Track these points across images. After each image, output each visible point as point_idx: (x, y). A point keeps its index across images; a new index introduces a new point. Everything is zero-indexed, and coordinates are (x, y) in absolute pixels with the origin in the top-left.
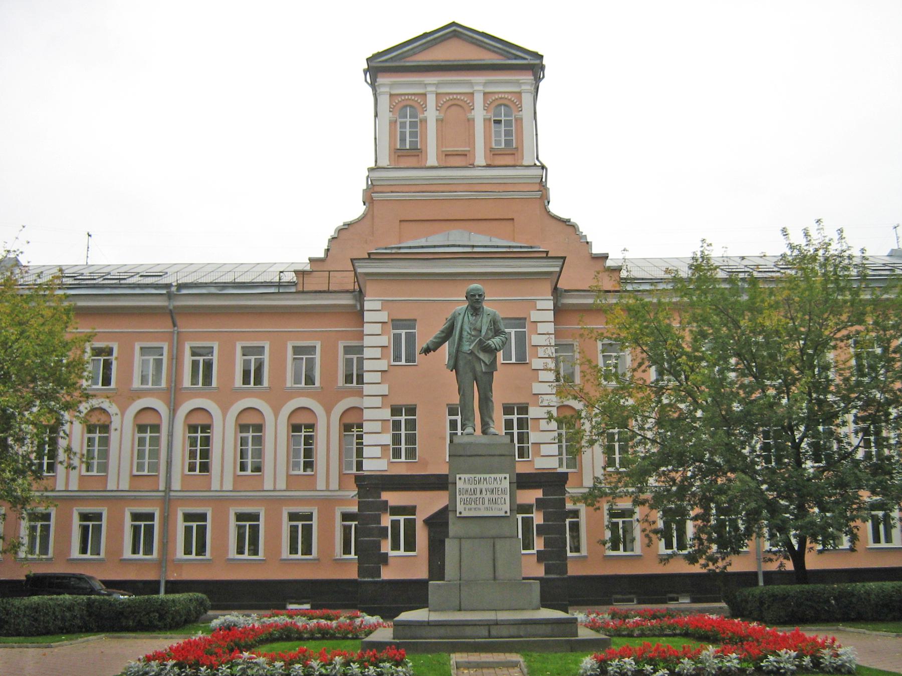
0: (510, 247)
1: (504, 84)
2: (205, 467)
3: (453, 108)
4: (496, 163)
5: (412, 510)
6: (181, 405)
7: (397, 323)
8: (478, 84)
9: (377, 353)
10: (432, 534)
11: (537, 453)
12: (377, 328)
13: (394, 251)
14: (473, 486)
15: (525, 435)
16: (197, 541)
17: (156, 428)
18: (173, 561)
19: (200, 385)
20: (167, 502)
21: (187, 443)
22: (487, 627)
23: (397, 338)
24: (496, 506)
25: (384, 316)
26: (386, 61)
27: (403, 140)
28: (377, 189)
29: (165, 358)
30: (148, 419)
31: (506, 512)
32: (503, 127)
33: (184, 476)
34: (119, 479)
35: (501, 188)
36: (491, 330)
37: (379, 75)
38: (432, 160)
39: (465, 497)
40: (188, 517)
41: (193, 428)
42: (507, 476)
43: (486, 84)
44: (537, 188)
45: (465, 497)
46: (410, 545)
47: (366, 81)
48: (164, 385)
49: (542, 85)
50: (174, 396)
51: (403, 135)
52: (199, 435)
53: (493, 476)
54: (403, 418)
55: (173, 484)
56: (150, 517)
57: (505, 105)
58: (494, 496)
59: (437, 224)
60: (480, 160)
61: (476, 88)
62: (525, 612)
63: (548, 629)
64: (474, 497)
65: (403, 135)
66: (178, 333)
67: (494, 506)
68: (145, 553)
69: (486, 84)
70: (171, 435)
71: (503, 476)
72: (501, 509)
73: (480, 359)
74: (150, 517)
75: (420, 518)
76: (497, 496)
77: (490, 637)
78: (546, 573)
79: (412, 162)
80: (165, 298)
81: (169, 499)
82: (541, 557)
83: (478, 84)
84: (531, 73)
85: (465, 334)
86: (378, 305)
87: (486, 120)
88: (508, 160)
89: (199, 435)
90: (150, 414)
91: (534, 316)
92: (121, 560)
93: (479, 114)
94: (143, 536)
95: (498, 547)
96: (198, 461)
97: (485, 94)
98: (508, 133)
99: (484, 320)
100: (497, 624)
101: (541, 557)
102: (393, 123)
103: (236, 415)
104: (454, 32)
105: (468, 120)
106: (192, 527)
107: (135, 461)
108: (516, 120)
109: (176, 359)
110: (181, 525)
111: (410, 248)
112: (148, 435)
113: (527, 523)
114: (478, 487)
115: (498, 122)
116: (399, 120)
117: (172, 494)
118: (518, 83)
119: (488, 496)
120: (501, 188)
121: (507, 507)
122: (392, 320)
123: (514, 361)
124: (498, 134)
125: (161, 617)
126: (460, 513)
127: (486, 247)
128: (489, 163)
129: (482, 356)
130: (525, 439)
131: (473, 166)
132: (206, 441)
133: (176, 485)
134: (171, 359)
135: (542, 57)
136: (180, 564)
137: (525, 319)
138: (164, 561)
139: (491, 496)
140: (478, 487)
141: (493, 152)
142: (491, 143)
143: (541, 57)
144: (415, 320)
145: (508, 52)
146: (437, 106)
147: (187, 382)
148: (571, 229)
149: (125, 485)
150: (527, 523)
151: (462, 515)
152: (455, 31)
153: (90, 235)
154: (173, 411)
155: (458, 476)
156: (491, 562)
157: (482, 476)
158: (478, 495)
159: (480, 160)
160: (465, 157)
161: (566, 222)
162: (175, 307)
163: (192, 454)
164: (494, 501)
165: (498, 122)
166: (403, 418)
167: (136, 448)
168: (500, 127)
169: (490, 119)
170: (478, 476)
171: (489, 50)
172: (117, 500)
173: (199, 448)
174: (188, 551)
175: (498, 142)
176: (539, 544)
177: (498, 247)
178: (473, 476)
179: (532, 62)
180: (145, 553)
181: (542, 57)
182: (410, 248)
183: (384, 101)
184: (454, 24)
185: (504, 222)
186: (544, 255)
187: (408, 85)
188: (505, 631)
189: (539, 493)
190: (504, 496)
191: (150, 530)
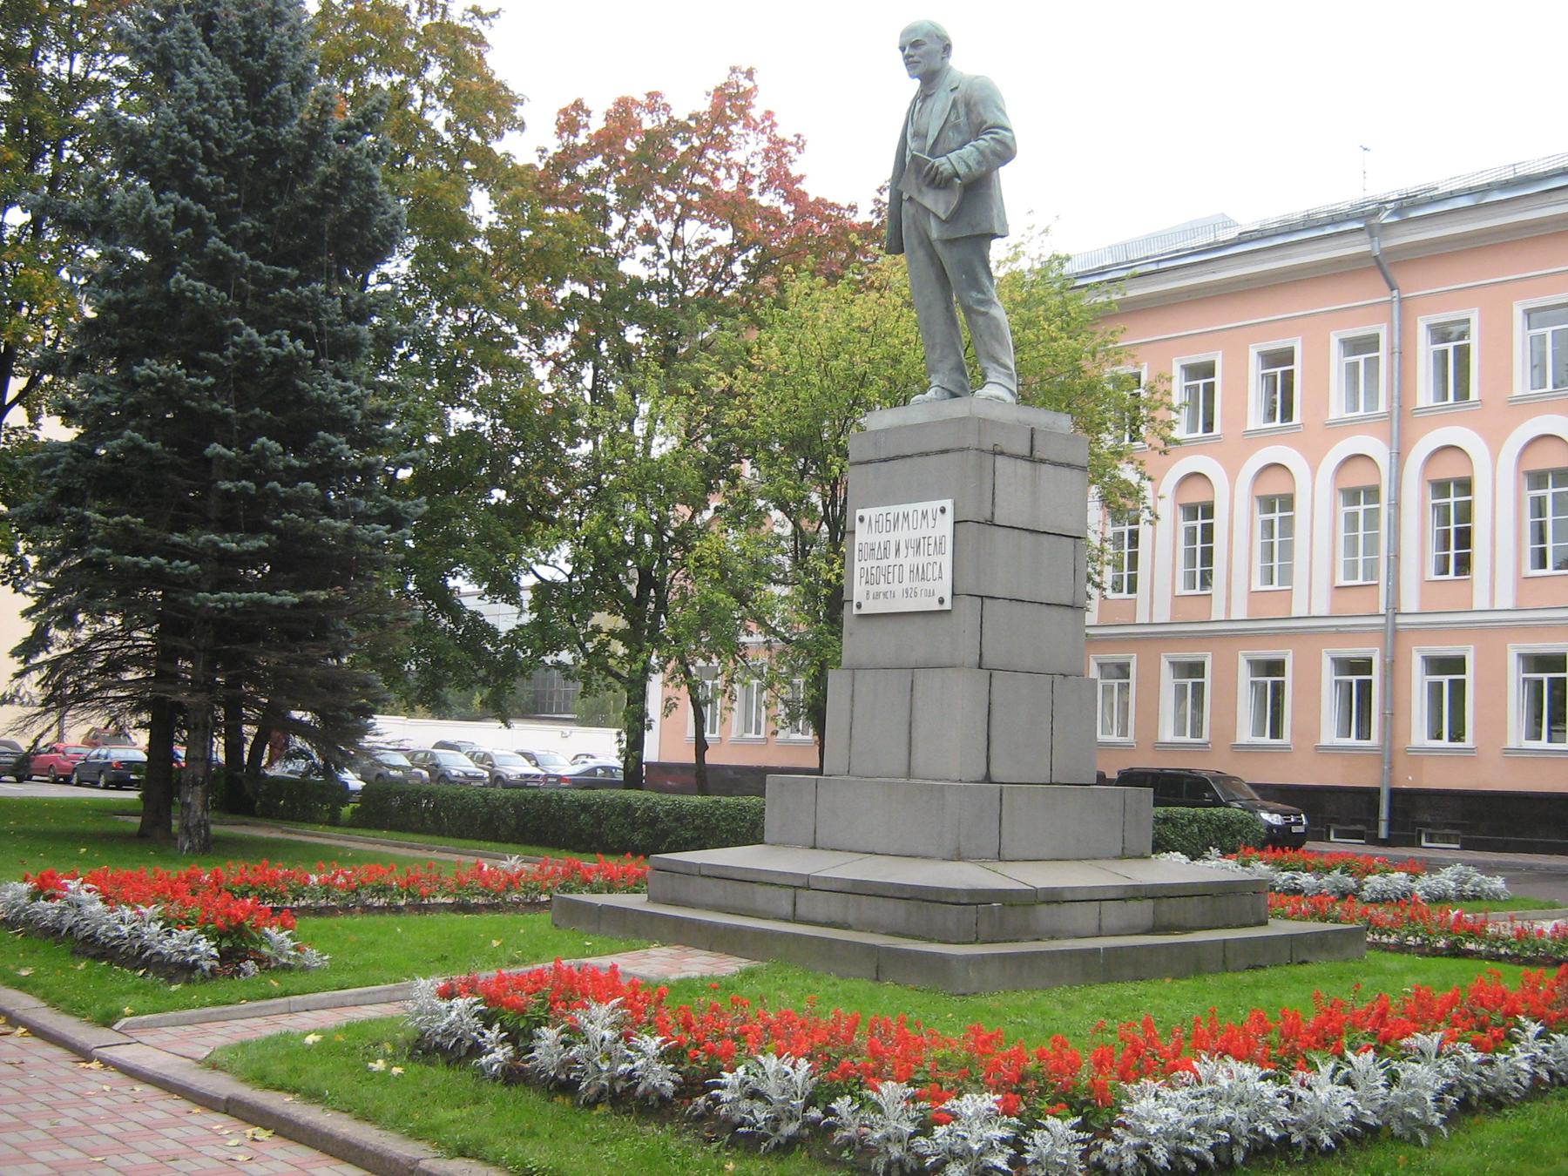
2: (1464, 564)
14: (884, 537)
15: (1536, 384)
16: (1450, 714)
17: (1372, 493)
19: (1550, 387)
20: (1394, 635)
21: (1431, 517)
22: (791, 891)
30: (1358, 477)
31: (941, 601)
34: (1311, 597)
36: (956, 127)
41: (1440, 488)
42: (948, 504)
48: (1382, 407)
50: (1401, 425)
52: (1452, 500)
58: (922, 560)
63: (894, 912)
64: (884, 563)
67: (921, 585)
68: (1359, 737)
70: (1396, 505)
71: (938, 504)
72: (931, 594)
77: (794, 919)
80: (1364, 237)
81: (1395, 631)
90: (1360, 465)
92: (1317, 748)
95: (918, 689)
96: (1452, 552)
100: (808, 888)
103: (1518, 450)
106: (1440, 684)
109: (1403, 354)
112: (1361, 508)
114: (893, 537)
119: (908, 560)
126: (859, 606)
136: (1422, 754)
138: (1389, 754)
140: (893, 537)
147: (1424, 394)
149: (1321, 606)
151: (863, 611)
154: (1399, 457)
162: (1387, 252)
164: (919, 573)
167: (1341, 534)
172: (1306, 633)
173: (1452, 527)
178: (883, 510)
180: (1359, 737)
191: (1365, 688)
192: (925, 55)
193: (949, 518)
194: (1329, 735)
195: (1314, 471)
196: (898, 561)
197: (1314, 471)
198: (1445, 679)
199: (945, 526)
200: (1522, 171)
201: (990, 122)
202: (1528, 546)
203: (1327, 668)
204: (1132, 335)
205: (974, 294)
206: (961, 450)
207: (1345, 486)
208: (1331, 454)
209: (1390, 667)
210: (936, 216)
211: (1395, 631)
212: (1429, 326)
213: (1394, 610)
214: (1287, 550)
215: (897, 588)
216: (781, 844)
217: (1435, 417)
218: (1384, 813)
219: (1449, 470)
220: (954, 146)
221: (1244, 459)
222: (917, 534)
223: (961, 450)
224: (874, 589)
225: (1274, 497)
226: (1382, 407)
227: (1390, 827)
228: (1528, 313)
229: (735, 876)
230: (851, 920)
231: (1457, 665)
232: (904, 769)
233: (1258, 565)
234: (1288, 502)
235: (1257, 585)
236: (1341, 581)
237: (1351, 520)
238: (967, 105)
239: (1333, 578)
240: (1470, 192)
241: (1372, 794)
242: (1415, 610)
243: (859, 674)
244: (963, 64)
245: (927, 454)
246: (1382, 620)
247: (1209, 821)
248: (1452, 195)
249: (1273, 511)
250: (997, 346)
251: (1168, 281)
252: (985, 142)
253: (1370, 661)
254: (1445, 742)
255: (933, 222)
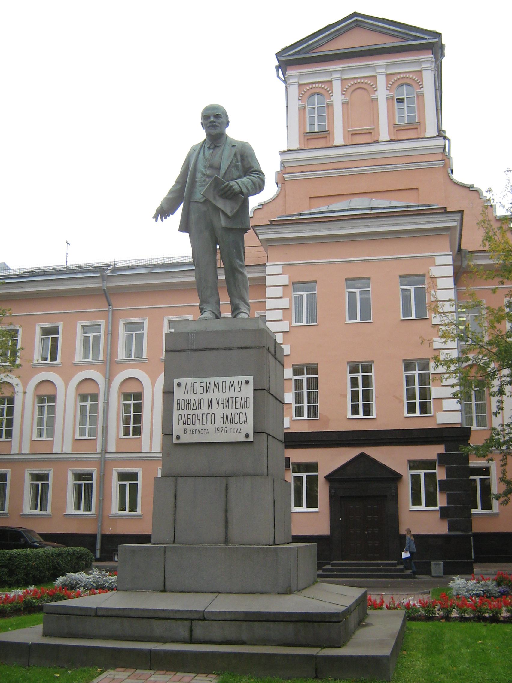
0: (408, 207)
1: (403, 65)
2: (137, 431)
3: (358, 91)
4: (400, 138)
5: (312, 467)
6: (116, 375)
7: (297, 285)
8: (380, 66)
9: (279, 315)
10: (333, 491)
11: (440, 408)
12: (279, 292)
13: (294, 218)
14: (198, 397)
16: (40, 496)
17: (95, 397)
18: (109, 516)
23: (299, 299)
24: (233, 426)
25: (285, 280)
26: (293, 54)
27: (312, 125)
28: (288, 170)
29: (102, 334)
30: (88, 389)
31: (247, 436)
32: (405, 104)
33: (119, 439)
34: (63, 442)
35: (405, 160)
36: (236, 167)
37: (288, 68)
38: (339, 139)
39: (186, 412)
40: (123, 477)
41: (126, 396)
42: (251, 378)
43: (387, 66)
44: (440, 157)
45: (186, 412)
46: (313, 502)
47: (278, 76)
48: (101, 358)
49: (445, 62)
50: (110, 367)
51: (312, 119)
53: (228, 379)
54: (305, 377)
55: (108, 448)
56: (90, 476)
57: (407, 84)
59: (345, 197)
60: (384, 135)
61: (378, 71)
62: (264, 598)
65: (312, 119)
66: (113, 311)
69: (387, 66)
70: (107, 403)
71: (244, 378)
72: (239, 431)
73: (217, 209)
74: (90, 476)
75: (322, 474)
76: (234, 411)
77: (191, 641)
78: (450, 530)
79: (321, 143)
80: (100, 280)
81: (105, 461)
82: (444, 513)
83: (380, 66)
84: (431, 51)
85: (199, 175)
86: (279, 269)
87: (389, 99)
88: (412, 134)
89: (132, 402)
91: (435, 271)
92: (65, 515)
93: (382, 94)
94: (84, 495)
96: (131, 425)
97: (387, 75)
98: (411, 109)
99: (226, 153)
100: (204, 619)
101: (444, 513)
102: (302, 110)
104: (356, 22)
105: (372, 100)
107: (78, 427)
108: (418, 96)
109: (112, 334)
110: (115, 484)
111: (311, 214)
113: (430, 478)
115: (400, 101)
116: (308, 107)
117: (108, 455)
118: (419, 62)
119: (221, 410)
120: (405, 160)
121: (249, 428)
122: (294, 283)
123: (414, 317)
124: (401, 110)
125: (11, 573)
126: (178, 437)
127: (384, 208)
128: (393, 138)
129: (220, 204)
130: (428, 396)
131: (377, 142)
132: (138, 408)
133: (112, 447)
134: (107, 334)
135: (440, 35)
137: (424, 275)
138: (100, 517)
139: (226, 411)
140: (206, 397)
141: (397, 128)
142: (394, 118)
143: (439, 35)
144: (315, 282)
145: (407, 34)
146: (342, 91)
148: (474, 194)
149: (68, 448)
150: (430, 478)
152: (357, 20)
153: (68, 244)
155: (176, 381)
156: (222, 514)
157: (212, 380)
158: (205, 410)
159: (384, 135)
160: (369, 135)
161: (470, 188)
162: (109, 288)
163: (127, 421)
164: (228, 419)
165: (400, 101)
166: (305, 377)
167: (78, 415)
168: (403, 106)
169: (392, 98)
170: (206, 380)
171: (389, 34)
172: (61, 461)
173: (132, 414)
174: (122, 508)
175: (401, 118)
176: (442, 501)
177: (396, 207)
178: (198, 380)
179: (431, 41)
181: (440, 35)
182: (311, 214)
183: (294, 90)
184: (355, 14)
185: (409, 192)
186: (443, 211)
187: (314, 74)
188: (216, 631)
189: (441, 449)
190: (244, 411)
191: (89, 487)
192: (214, 121)
193: (251, 386)
194: (70, 509)
195: (66, 385)
196: (211, 411)
197: (66, 385)
198: (128, 483)
199: (248, 392)
200: (168, 262)
201: (255, 168)
202: (122, 425)
203: (70, 477)
204: (18, 311)
205: (238, 261)
206: (258, 348)
207: (81, 393)
208: (144, 374)
209: (103, 478)
210: (224, 213)
211: (105, 461)
212: (41, 328)
213: (105, 450)
214: (51, 422)
215: (209, 426)
216: (136, 590)
217: (127, 364)
218: (98, 546)
219: (132, 388)
220: (235, 177)
221: (73, 375)
222: (227, 395)
223: (258, 348)
224: (190, 427)
225: (45, 396)
226: (101, 358)
227: (101, 552)
228: (83, 327)
229: (132, 614)
230: (245, 637)
231: (133, 476)
232: (222, 538)
233: (35, 427)
234: (52, 399)
235: (35, 438)
236: (77, 437)
237: (83, 409)
238: (242, 156)
239: (31, 437)
240: (145, 267)
241: (94, 536)
242: (114, 451)
243: (180, 480)
244: (234, 132)
245: (230, 349)
246: (99, 456)
247: (74, 554)
248: (138, 267)
249: (4, 404)
250: (246, 293)
251: (48, 286)
252: (255, 178)
253: (48, 474)
254: (127, 512)
255: (222, 217)
